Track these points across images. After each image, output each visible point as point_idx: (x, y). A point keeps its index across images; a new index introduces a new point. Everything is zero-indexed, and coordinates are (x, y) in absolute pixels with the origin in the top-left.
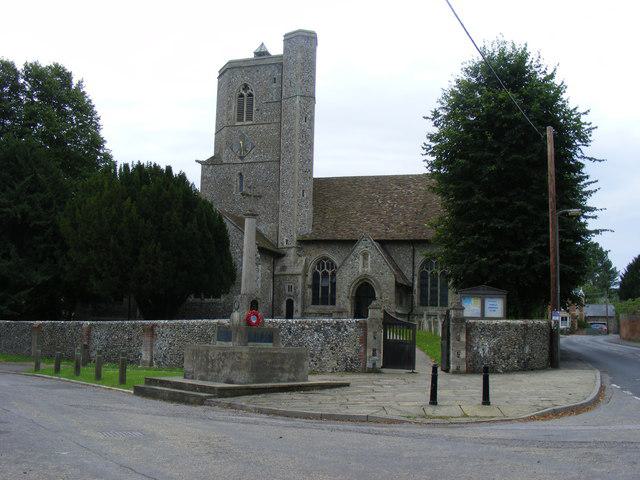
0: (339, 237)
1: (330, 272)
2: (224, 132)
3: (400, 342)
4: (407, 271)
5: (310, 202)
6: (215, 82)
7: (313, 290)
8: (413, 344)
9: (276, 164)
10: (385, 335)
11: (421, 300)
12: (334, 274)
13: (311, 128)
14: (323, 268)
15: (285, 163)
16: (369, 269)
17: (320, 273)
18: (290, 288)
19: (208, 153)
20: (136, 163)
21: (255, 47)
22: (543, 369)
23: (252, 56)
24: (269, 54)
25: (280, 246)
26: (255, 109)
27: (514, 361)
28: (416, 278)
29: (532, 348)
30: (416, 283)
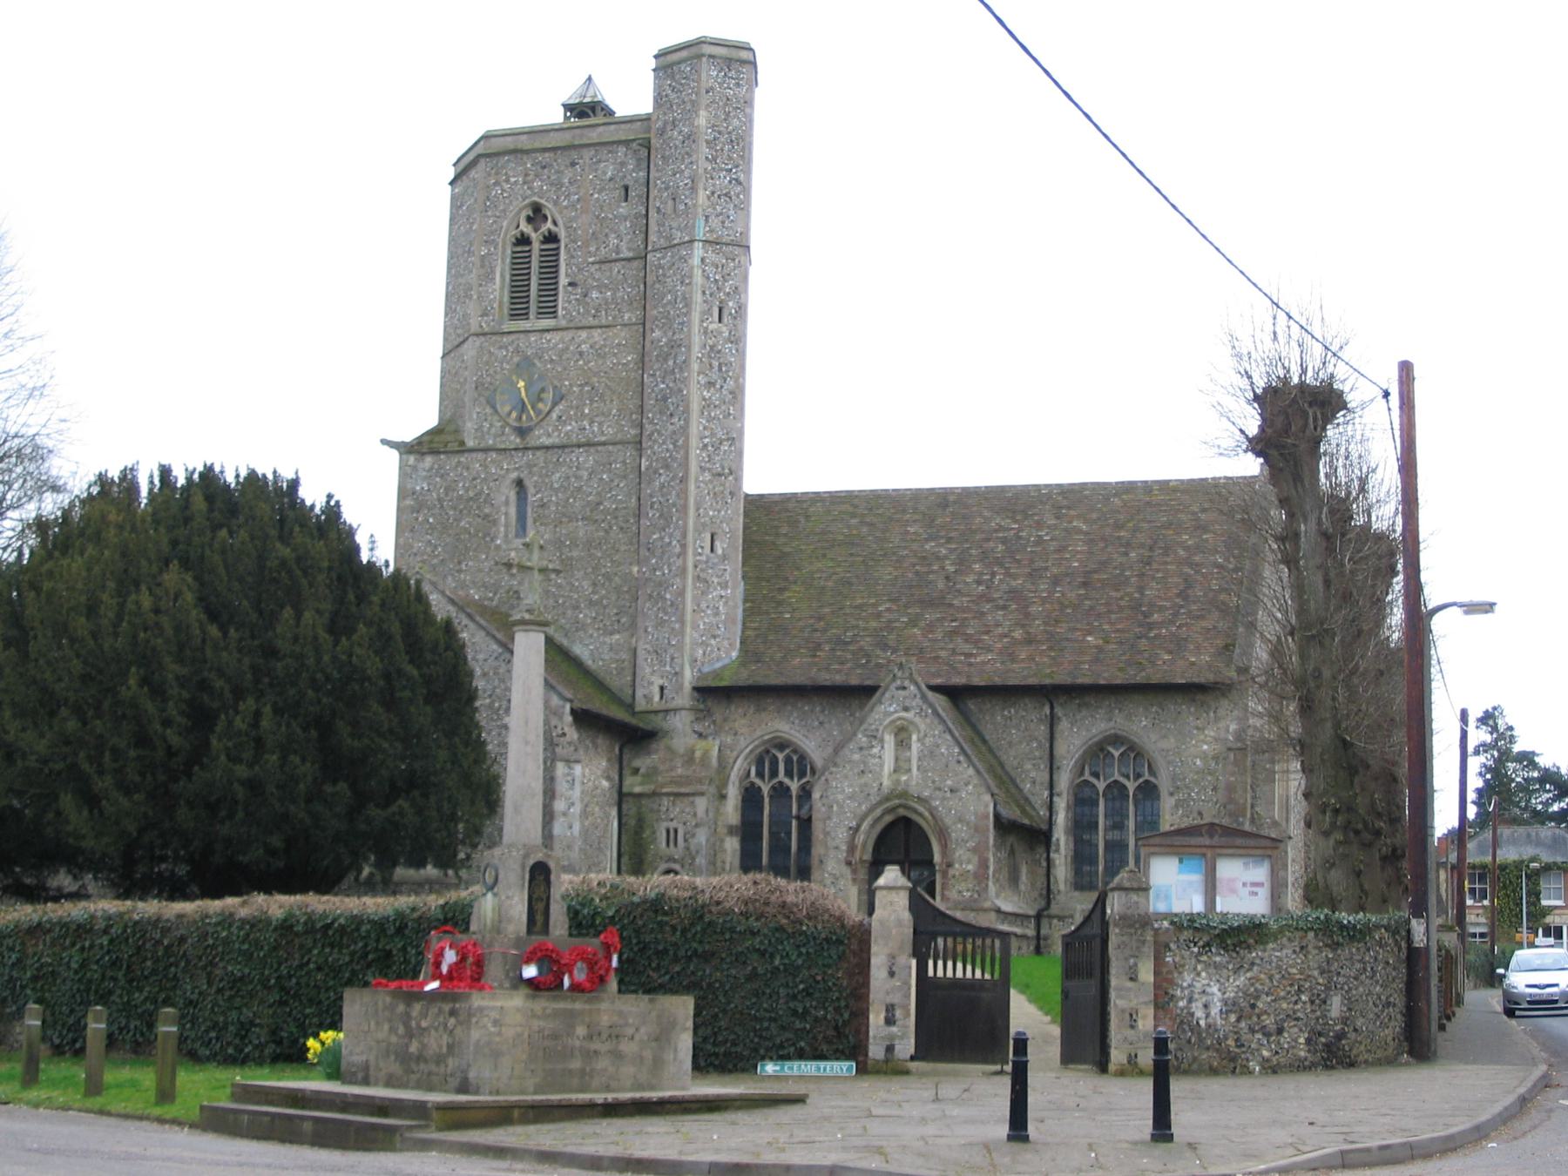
0: (825, 678)
1: (794, 786)
2: (470, 350)
3: (972, 985)
4: (1032, 779)
5: (733, 569)
6: (442, 197)
7: (744, 841)
8: (1003, 984)
9: (630, 452)
10: (922, 969)
11: (1078, 872)
12: (806, 794)
13: (737, 339)
14: (774, 773)
15: (658, 447)
16: (913, 779)
17: (766, 789)
18: (672, 836)
19: (423, 417)
20: (243, 473)
21: (569, 90)
22: (1390, 1062)
23: (555, 116)
24: (611, 113)
25: (641, 705)
26: (563, 280)
27: (1297, 1040)
28: (1061, 804)
29: (1350, 1004)
30: (1061, 818)
